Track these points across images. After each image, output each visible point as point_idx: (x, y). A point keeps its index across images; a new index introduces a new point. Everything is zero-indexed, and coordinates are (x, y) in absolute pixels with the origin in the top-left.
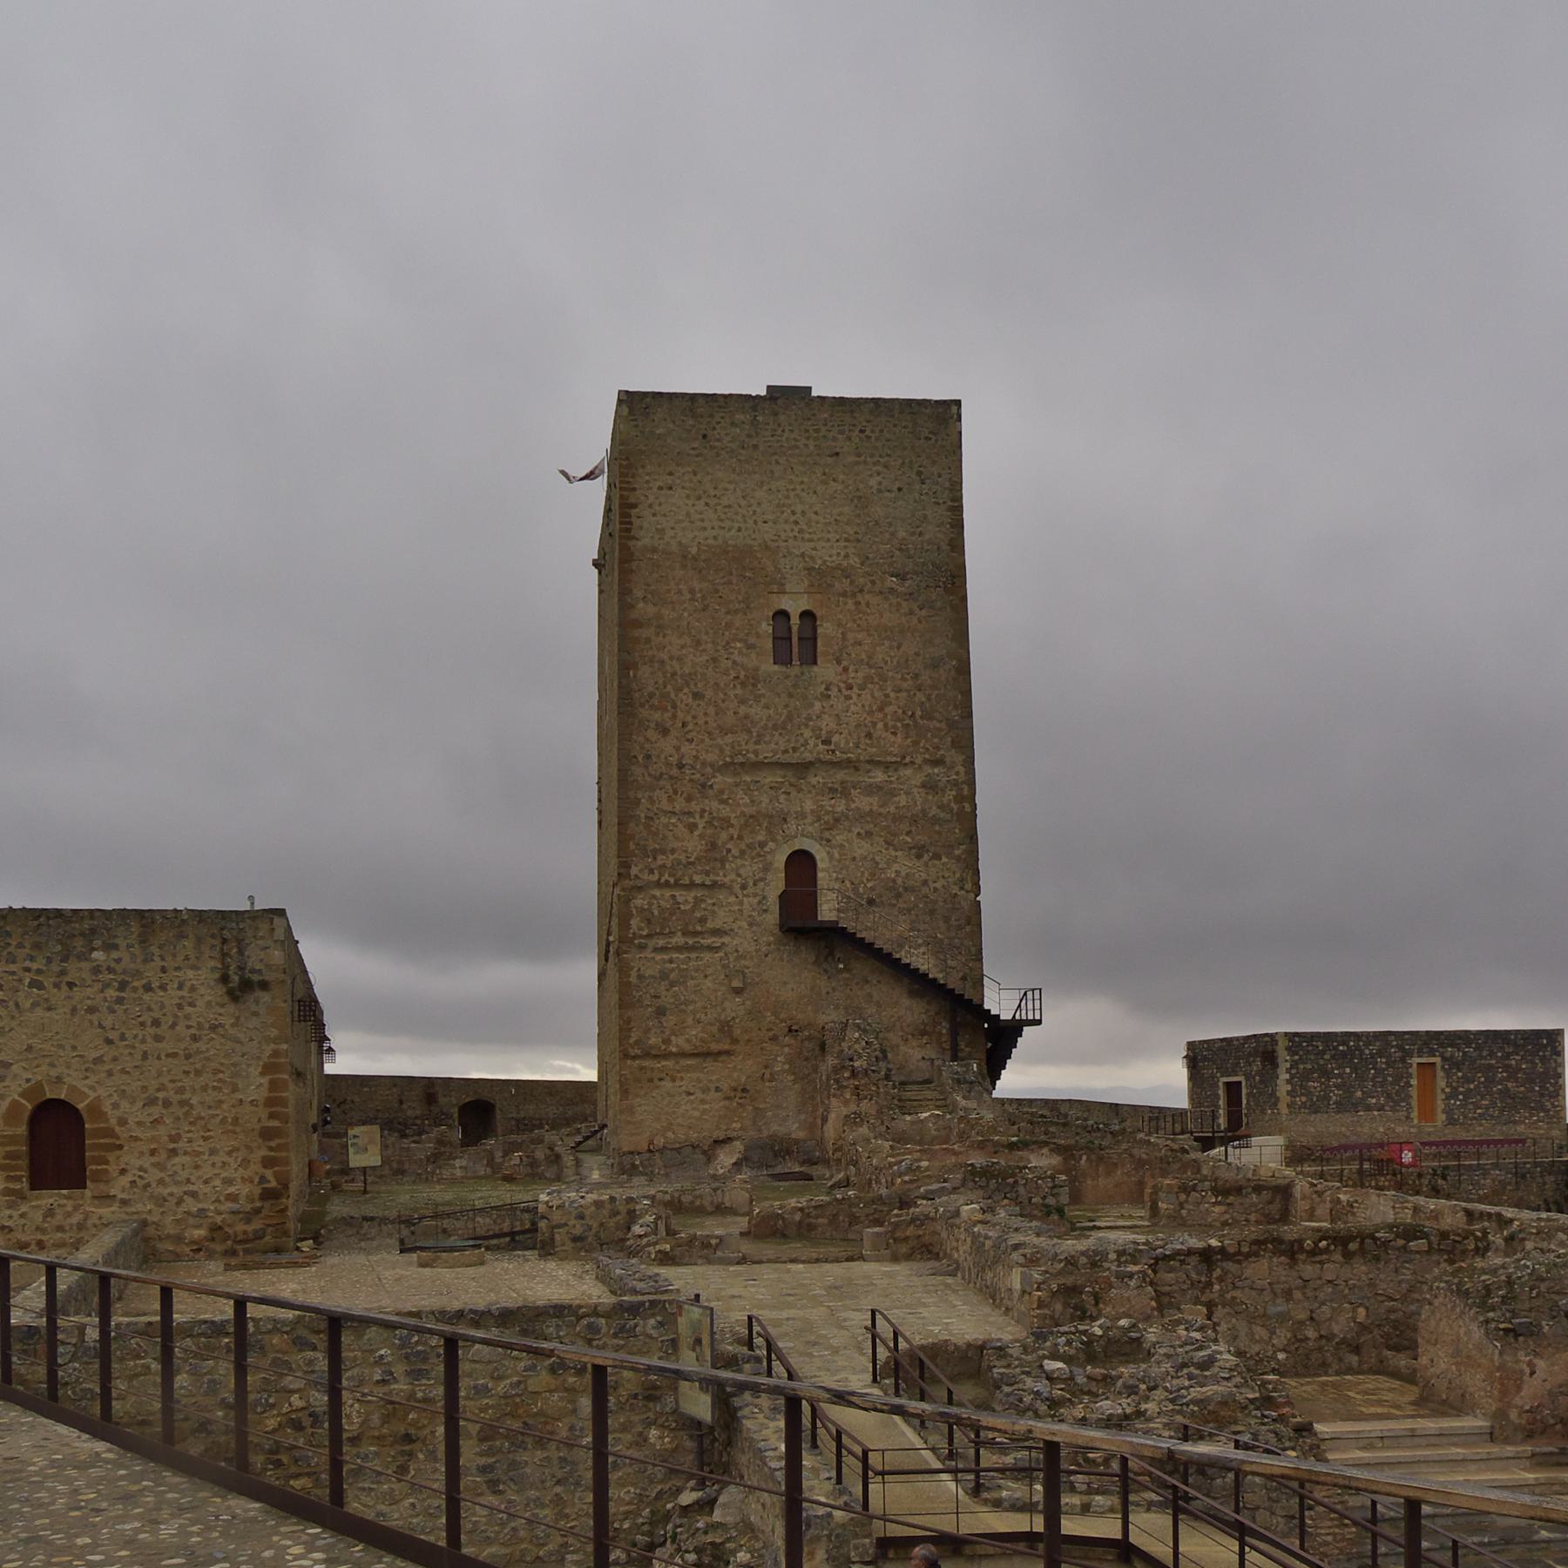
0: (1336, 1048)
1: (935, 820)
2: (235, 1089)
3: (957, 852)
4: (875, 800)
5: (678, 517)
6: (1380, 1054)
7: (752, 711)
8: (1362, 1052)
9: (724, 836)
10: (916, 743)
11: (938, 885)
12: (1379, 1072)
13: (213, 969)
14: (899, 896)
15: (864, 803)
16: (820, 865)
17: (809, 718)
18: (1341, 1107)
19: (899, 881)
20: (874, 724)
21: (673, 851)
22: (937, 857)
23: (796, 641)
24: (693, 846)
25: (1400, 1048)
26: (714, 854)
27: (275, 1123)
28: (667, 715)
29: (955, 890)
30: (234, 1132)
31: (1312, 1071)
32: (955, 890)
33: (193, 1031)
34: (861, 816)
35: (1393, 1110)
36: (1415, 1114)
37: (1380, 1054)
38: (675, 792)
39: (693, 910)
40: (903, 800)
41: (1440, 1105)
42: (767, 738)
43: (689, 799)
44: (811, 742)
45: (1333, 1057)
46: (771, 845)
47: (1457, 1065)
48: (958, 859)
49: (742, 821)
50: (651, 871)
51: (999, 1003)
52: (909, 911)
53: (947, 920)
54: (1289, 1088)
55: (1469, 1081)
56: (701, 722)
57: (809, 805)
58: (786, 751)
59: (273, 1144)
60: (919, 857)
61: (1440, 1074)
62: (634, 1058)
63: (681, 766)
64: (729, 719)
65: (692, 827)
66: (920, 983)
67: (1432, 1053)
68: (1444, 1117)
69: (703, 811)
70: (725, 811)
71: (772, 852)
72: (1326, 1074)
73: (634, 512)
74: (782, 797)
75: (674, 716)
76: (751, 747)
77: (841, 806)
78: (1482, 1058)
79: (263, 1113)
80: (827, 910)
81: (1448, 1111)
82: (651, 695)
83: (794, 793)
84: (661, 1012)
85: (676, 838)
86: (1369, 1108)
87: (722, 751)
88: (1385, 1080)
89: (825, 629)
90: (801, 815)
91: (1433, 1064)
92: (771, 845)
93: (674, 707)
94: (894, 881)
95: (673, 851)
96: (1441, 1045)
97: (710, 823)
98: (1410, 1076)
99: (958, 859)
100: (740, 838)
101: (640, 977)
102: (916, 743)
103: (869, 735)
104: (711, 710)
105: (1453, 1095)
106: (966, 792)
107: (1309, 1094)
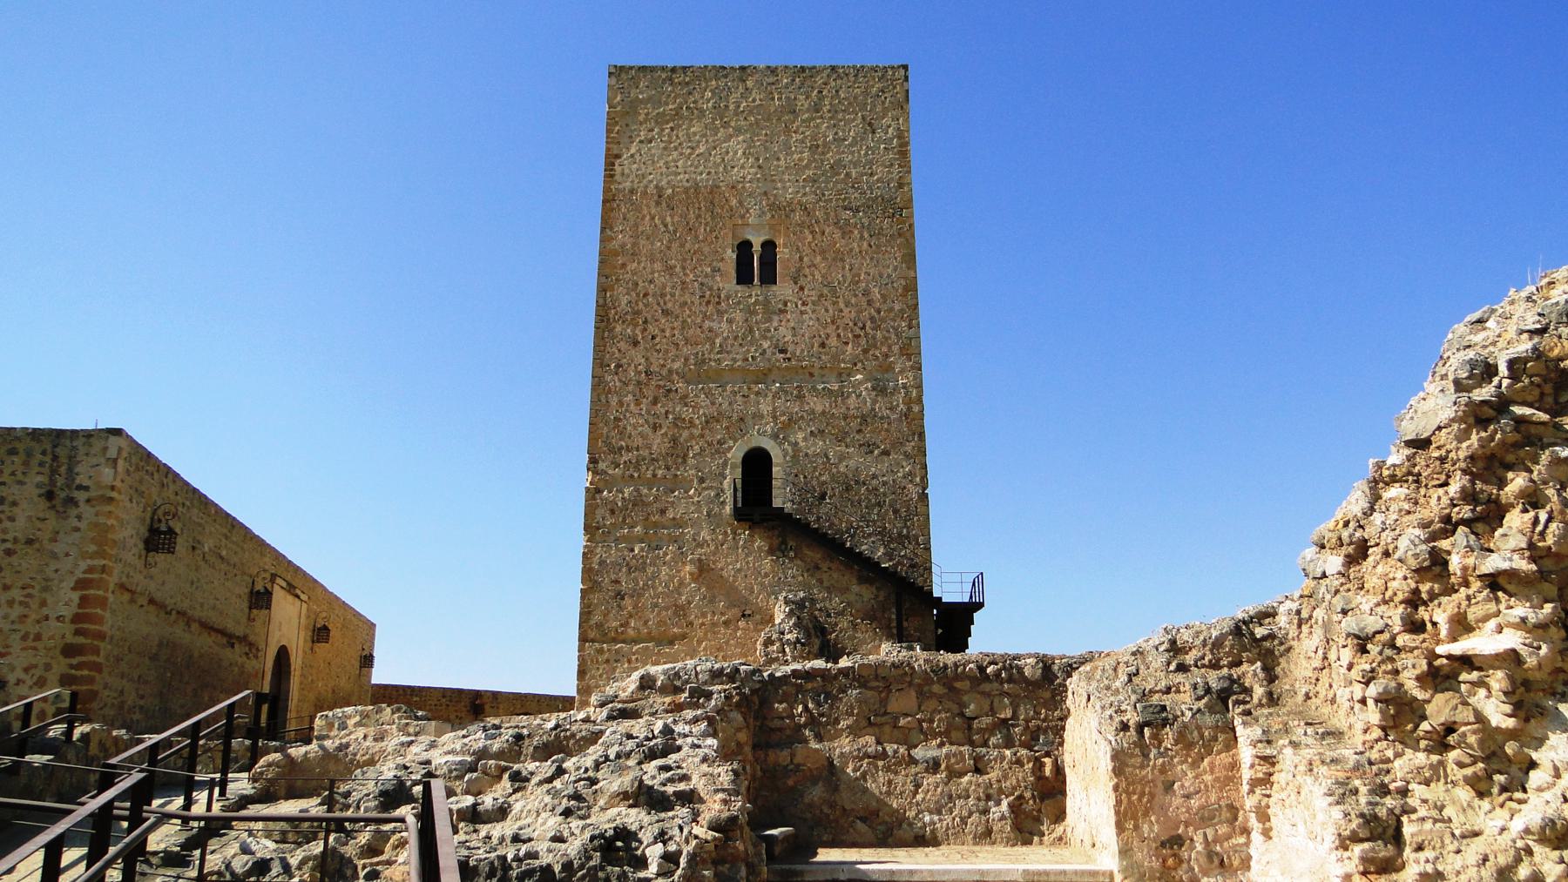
2: (43, 603)
5: (658, 163)
9: (685, 434)
13: (38, 486)
15: (818, 405)
23: (756, 265)
24: (658, 443)
26: (677, 452)
27: (81, 640)
30: (35, 649)
33: (8, 545)
50: (618, 466)
51: (948, 588)
59: (75, 661)
62: (593, 641)
66: (866, 568)
73: (617, 162)
79: (68, 629)
80: (781, 498)
84: (620, 596)
89: (782, 253)
102: (865, 351)
103: (823, 345)
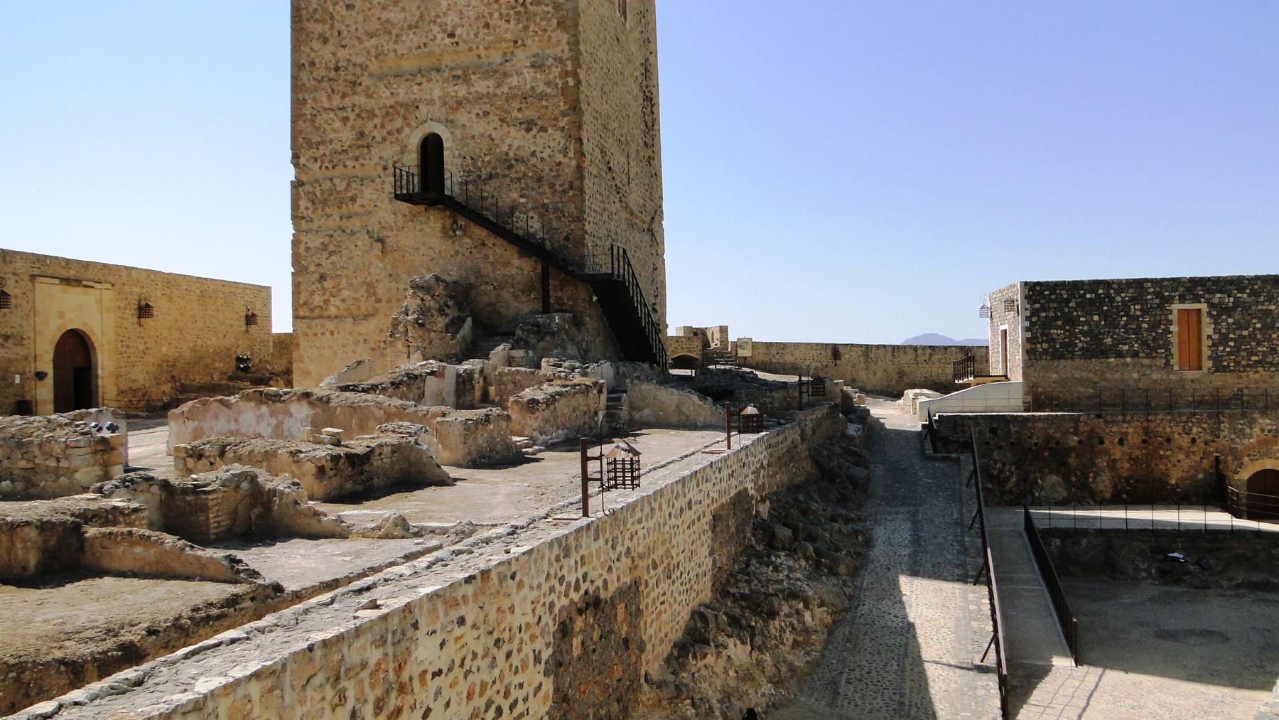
0: (1083, 296)
1: (542, 96)
3: (562, 124)
4: (491, 83)
6: (1134, 300)
7: (391, 15)
8: (1112, 300)
9: (370, 126)
10: (526, 28)
11: (545, 155)
12: (1132, 318)
14: (510, 167)
16: (445, 145)
17: (437, 16)
18: (1088, 354)
19: (511, 154)
20: (491, 15)
21: (331, 142)
22: (543, 129)
24: (347, 135)
25: (1158, 294)
28: (327, 26)
29: (560, 158)
31: (1056, 318)
32: (560, 158)
34: (479, 98)
35: (1148, 356)
36: (1174, 361)
37: (1134, 300)
38: (333, 91)
39: (346, 190)
40: (514, 81)
41: (1206, 352)
42: (404, 38)
43: (344, 96)
44: (439, 36)
45: (1078, 305)
46: (407, 130)
47: (1228, 311)
48: (563, 129)
49: (384, 111)
52: (519, 179)
53: (552, 186)
54: (1170, 317)
55: (1241, 328)
56: (352, 29)
57: (437, 93)
58: (419, 47)
60: (528, 130)
61: (1206, 320)
63: (337, 69)
64: (374, 25)
65: (345, 120)
67: (1197, 299)
68: (1210, 364)
69: (354, 105)
70: (371, 104)
71: (408, 136)
72: (1070, 321)
74: (416, 88)
75: (332, 27)
76: (391, 46)
77: (462, 91)
78: (1257, 303)
81: (1216, 359)
82: (315, 10)
83: (425, 84)
85: (334, 131)
86: (1120, 355)
87: (368, 53)
88: (1139, 327)
90: (431, 102)
91: (1199, 310)
92: (407, 130)
93: (332, 18)
94: (507, 154)
95: (331, 142)
96: (1208, 291)
97: (359, 115)
98: (1171, 322)
99: (563, 129)
100: (383, 126)
101: (308, 249)
102: (526, 28)
103: (487, 26)
104: (360, 19)
105: (1224, 340)
106: (569, 68)
107: (1051, 340)
